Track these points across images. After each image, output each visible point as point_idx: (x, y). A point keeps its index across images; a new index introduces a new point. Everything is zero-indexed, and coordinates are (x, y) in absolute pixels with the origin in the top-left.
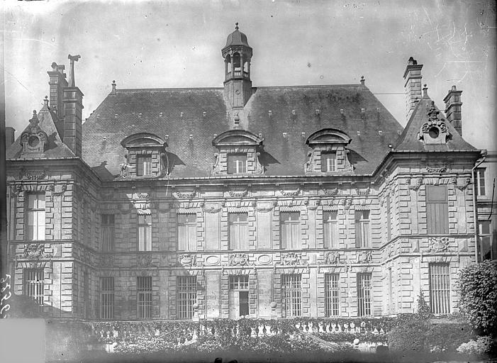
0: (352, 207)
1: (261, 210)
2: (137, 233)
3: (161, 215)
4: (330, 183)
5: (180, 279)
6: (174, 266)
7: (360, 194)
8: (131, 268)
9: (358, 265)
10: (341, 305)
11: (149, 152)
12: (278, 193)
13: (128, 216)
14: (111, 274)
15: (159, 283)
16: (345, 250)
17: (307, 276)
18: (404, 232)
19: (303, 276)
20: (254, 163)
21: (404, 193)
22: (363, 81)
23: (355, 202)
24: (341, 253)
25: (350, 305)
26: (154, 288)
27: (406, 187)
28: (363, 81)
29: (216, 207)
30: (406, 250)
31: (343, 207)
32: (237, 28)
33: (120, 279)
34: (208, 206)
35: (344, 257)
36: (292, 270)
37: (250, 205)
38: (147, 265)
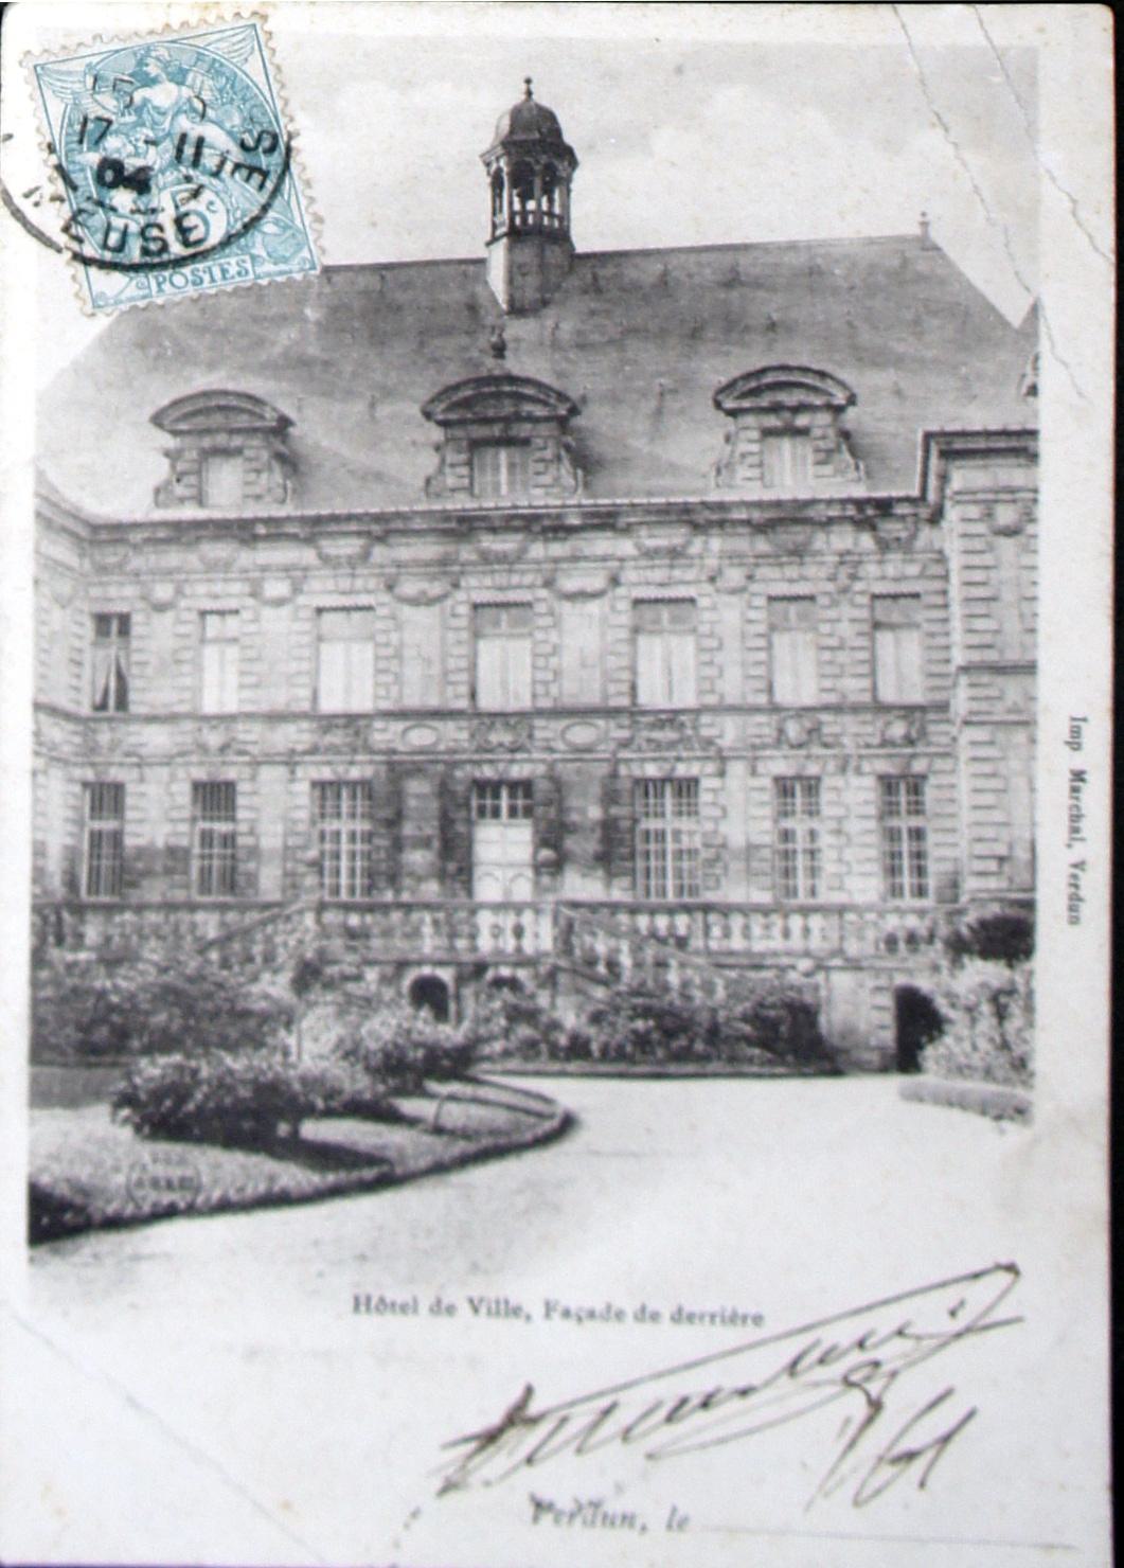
0: (858, 586)
1: (414, 602)
2: (198, 667)
3: (268, 613)
4: (785, 520)
5: (646, 787)
6: (305, 753)
7: (884, 546)
8: (752, 754)
9: (882, 751)
10: (829, 866)
11: (237, 441)
12: (626, 546)
13: (169, 616)
14: (115, 774)
15: (256, 800)
16: (836, 709)
17: (715, 783)
18: (976, 656)
19: (705, 783)
20: (553, 469)
21: (978, 544)
22: (925, 225)
23: (871, 569)
24: (825, 717)
25: (856, 868)
26: (241, 814)
27: (981, 528)
28: (925, 225)
29: (436, 589)
30: (984, 706)
31: (830, 587)
32: (529, 93)
33: (142, 788)
34: (409, 587)
35: (836, 729)
36: (667, 766)
37: (539, 581)
38: (223, 749)
